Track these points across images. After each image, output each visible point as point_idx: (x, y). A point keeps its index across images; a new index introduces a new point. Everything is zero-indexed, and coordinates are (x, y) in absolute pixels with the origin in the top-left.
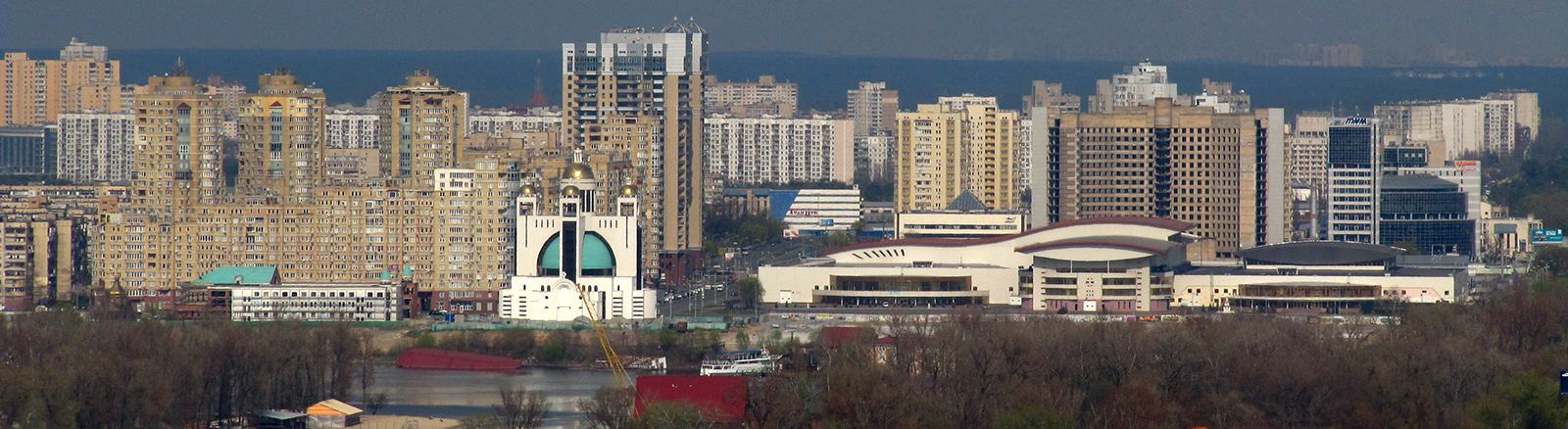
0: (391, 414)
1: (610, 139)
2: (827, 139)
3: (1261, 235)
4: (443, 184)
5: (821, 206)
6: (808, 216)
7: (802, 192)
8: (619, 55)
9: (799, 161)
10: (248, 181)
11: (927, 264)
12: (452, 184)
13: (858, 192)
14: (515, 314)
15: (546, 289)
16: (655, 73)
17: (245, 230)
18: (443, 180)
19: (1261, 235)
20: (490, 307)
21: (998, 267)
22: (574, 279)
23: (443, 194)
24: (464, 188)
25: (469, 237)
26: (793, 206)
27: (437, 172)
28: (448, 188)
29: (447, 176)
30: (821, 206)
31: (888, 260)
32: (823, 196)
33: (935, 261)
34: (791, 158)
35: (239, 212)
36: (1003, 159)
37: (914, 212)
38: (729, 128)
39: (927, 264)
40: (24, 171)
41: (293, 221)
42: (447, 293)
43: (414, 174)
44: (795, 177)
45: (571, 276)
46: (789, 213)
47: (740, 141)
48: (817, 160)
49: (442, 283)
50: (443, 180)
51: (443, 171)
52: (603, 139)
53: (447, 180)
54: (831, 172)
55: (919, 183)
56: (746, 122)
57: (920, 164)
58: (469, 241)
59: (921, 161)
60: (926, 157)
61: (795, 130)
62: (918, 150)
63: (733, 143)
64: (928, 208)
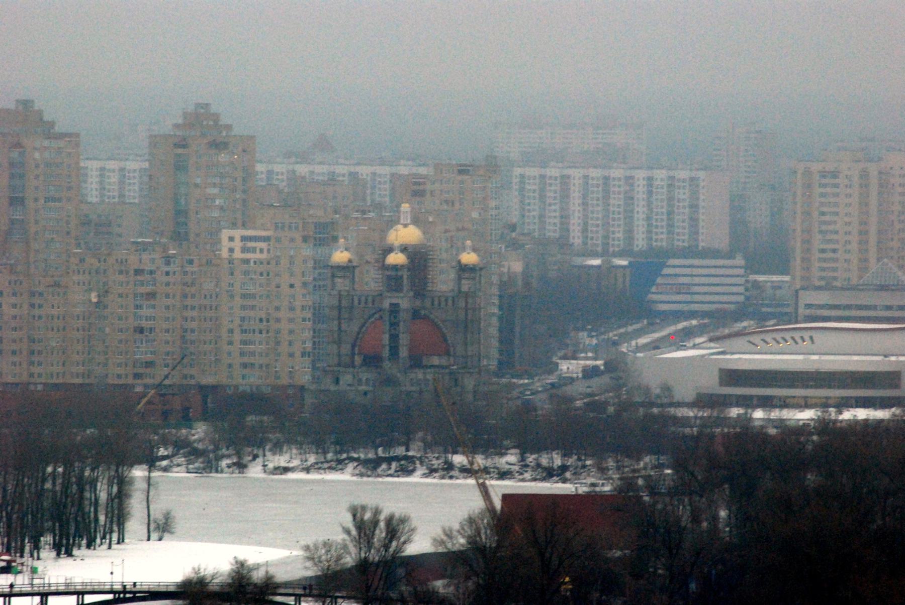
0: (825, 373)
2: (694, 195)
4: (231, 250)
5: (697, 280)
7: (671, 262)
12: (244, 250)
13: (742, 262)
21: (123, 574)
24: (258, 256)
27: (225, 234)
28: (238, 254)
30: (697, 280)
32: (698, 267)
36: (866, 223)
43: (192, 237)
44: (655, 244)
46: (654, 289)
49: (231, 377)
50: (232, 244)
53: (237, 244)
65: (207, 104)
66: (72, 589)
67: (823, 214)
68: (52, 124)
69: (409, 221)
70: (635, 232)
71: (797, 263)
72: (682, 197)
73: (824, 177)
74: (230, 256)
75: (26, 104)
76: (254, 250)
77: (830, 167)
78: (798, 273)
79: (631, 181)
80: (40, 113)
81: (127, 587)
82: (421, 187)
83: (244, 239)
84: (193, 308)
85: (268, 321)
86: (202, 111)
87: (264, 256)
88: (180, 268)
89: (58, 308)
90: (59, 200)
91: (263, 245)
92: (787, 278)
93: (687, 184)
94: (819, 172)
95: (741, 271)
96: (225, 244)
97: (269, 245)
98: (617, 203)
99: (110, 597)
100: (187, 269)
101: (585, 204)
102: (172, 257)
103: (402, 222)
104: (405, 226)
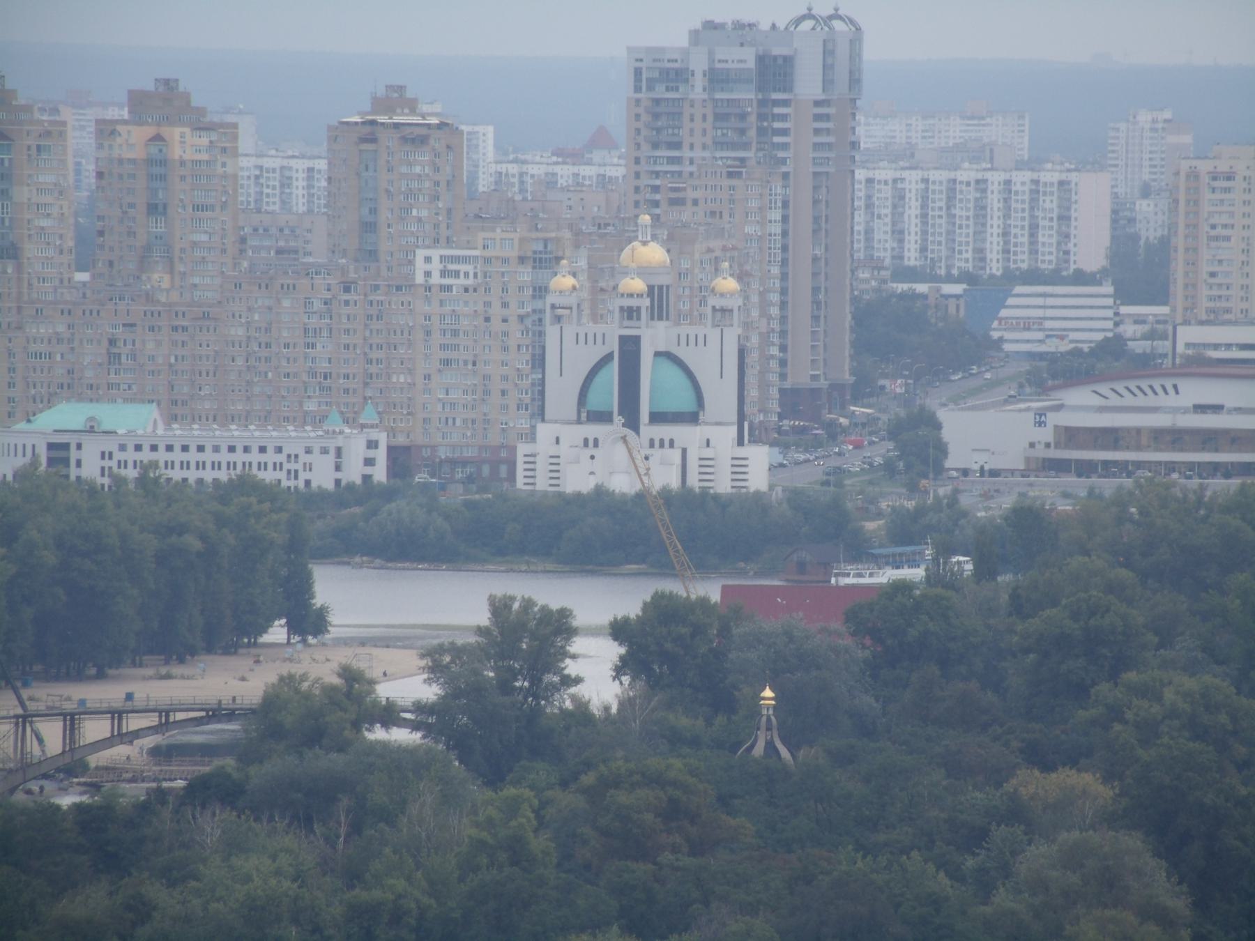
1: (701, 203)
3: (1110, 307)
4: (428, 274)
5: (1049, 313)
6: (1028, 329)
7: (1019, 289)
8: (718, 65)
9: (1020, 240)
10: (111, 264)
11: (1217, 409)
12: (444, 273)
14: (542, 484)
15: (591, 443)
16: (775, 96)
17: (105, 343)
18: (428, 267)
19: (1110, 307)
20: (503, 470)
22: (636, 428)
23: (428, 288)
24: (462, 281)
25: (471, 359)
26: (1004, 313)
27: (421, 254)
28: (436, 279)
29: (436, 260)
30: (1049, 313)
31: (1151, 400)
33: (1229, 403)
34: (1005, 234)
35: (95, 313)
37: (1202, 323)
38: (906, 185)
39: (1217, 409)
40: (818, 341)
41: (185, 329)
42: (434, 448)
45: (633, 423)
46: (995, 324)
47: (924, 206)
48: (1047, 238)
51: (428, 252)
52: (689, 203)
53: (436, 266)
54: (1072, 258)
55: (1213, 275)
56: (934, 175)
57: (1213, 244)
58: (470, 367)
59: (1217, 238)
60: (1225, 232)
61: (1014, 188)
62: (1212, 221)
63: (912, 210)
64: (1227, 316)
65: (401, 87)
66: (152, 704)
67: (1213, 227)
68: (201, 111)
69: (649, 238)
70: (988, 250)
71: (1178, 290)
72: (1048, 205)
73: (1215, 179)
74: (426, 281)
75: (169, 84)
76: (457, 274)
77: (1223, 167)
78: (1180, 303)
79: (982, 186)
80: (186, 96)
81: (223, 702)
82: (681, 195)
83: (443, 258)
84: (380, 347)
85: (474, 364)
86: (396, 95)
87: (470, 282)
88: (362, 297)
89: (208, 346)
90: (212, 208)
91: (469, 268)
92: (1164, 310)
93: (1055, 189)
94: (1209, 173)
95: (1110, 301)
96: (420, 267)
97: (476, 267)
98: (964, 213)
99: (203, 714)
100: (371, 298)
101: (924, 216)
102: (352, 283)
103: (640, 238)
104: (645, 243)
